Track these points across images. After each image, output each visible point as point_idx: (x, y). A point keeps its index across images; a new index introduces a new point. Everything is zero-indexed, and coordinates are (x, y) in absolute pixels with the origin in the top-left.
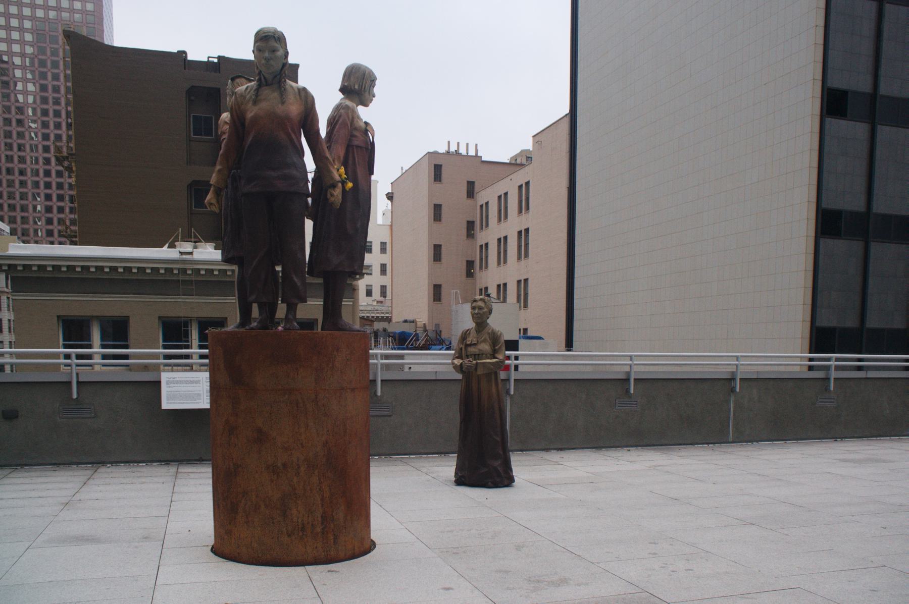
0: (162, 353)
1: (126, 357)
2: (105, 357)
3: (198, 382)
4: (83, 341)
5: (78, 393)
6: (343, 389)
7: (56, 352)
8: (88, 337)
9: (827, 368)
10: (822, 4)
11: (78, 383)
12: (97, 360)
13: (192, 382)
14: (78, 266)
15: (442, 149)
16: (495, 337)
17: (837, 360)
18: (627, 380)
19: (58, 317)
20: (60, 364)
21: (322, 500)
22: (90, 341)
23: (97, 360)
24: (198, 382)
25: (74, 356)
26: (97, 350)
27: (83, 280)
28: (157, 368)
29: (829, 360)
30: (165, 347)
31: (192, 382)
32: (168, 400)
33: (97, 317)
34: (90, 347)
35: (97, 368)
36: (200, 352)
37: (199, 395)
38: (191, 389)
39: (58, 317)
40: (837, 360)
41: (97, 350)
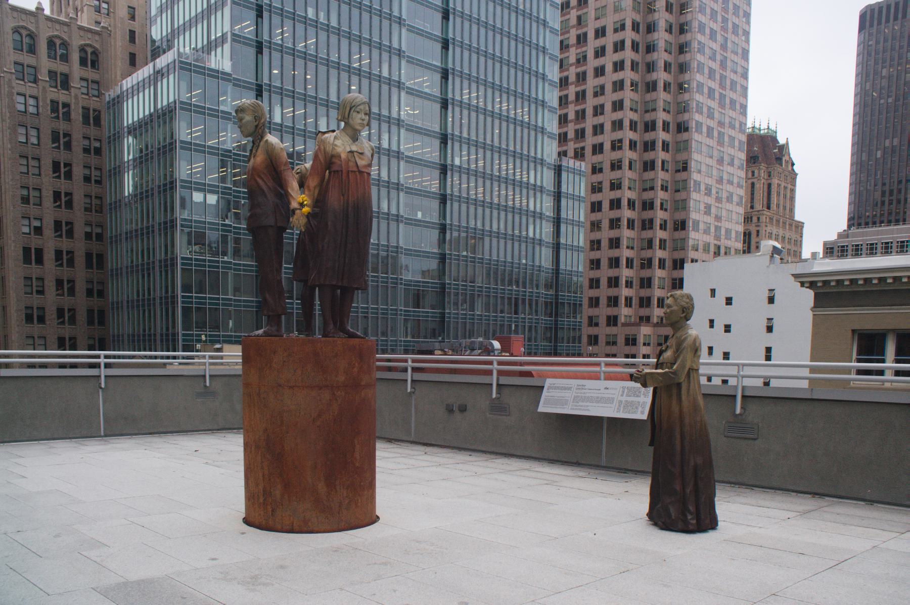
0: (853, 367)
1: (222, 358)
2: (898, 373)
3: (570, 389)
4: (873, 355)
5: (106, 383)
6: (280, 386)
7: (845, 366)
8: (882, 352)
9: (204, 364)
10: (304, 1)
11: (743, 397)
12: (889, 376)
13: (565, 389)
14: (875, 278)
15: (782, 141)
16: (697, 345)
17: (106, 357)
18: (204, 376)
19: (853, 331)
20: (849, 381)
21: (263, 476)
22: (883, 355)
23: (889, 376)
24: (570, 389)
25: (102, 357)
26: (890, 364)
27: (896, 291)
28: (544, 376)
29: (98, 357)
30: (859, 361)
31: (565, 389)
32: (544, 404)
33: (893, 330)
34: (883, 361)
35: (887, 385)
36: (859, 366)
37: (567, 401)
38: (563, 395)
39: (853, 331)
40: (106, 357)
41: (890, 364)
